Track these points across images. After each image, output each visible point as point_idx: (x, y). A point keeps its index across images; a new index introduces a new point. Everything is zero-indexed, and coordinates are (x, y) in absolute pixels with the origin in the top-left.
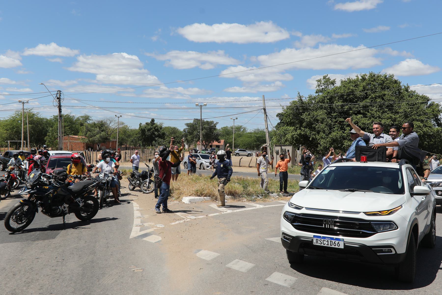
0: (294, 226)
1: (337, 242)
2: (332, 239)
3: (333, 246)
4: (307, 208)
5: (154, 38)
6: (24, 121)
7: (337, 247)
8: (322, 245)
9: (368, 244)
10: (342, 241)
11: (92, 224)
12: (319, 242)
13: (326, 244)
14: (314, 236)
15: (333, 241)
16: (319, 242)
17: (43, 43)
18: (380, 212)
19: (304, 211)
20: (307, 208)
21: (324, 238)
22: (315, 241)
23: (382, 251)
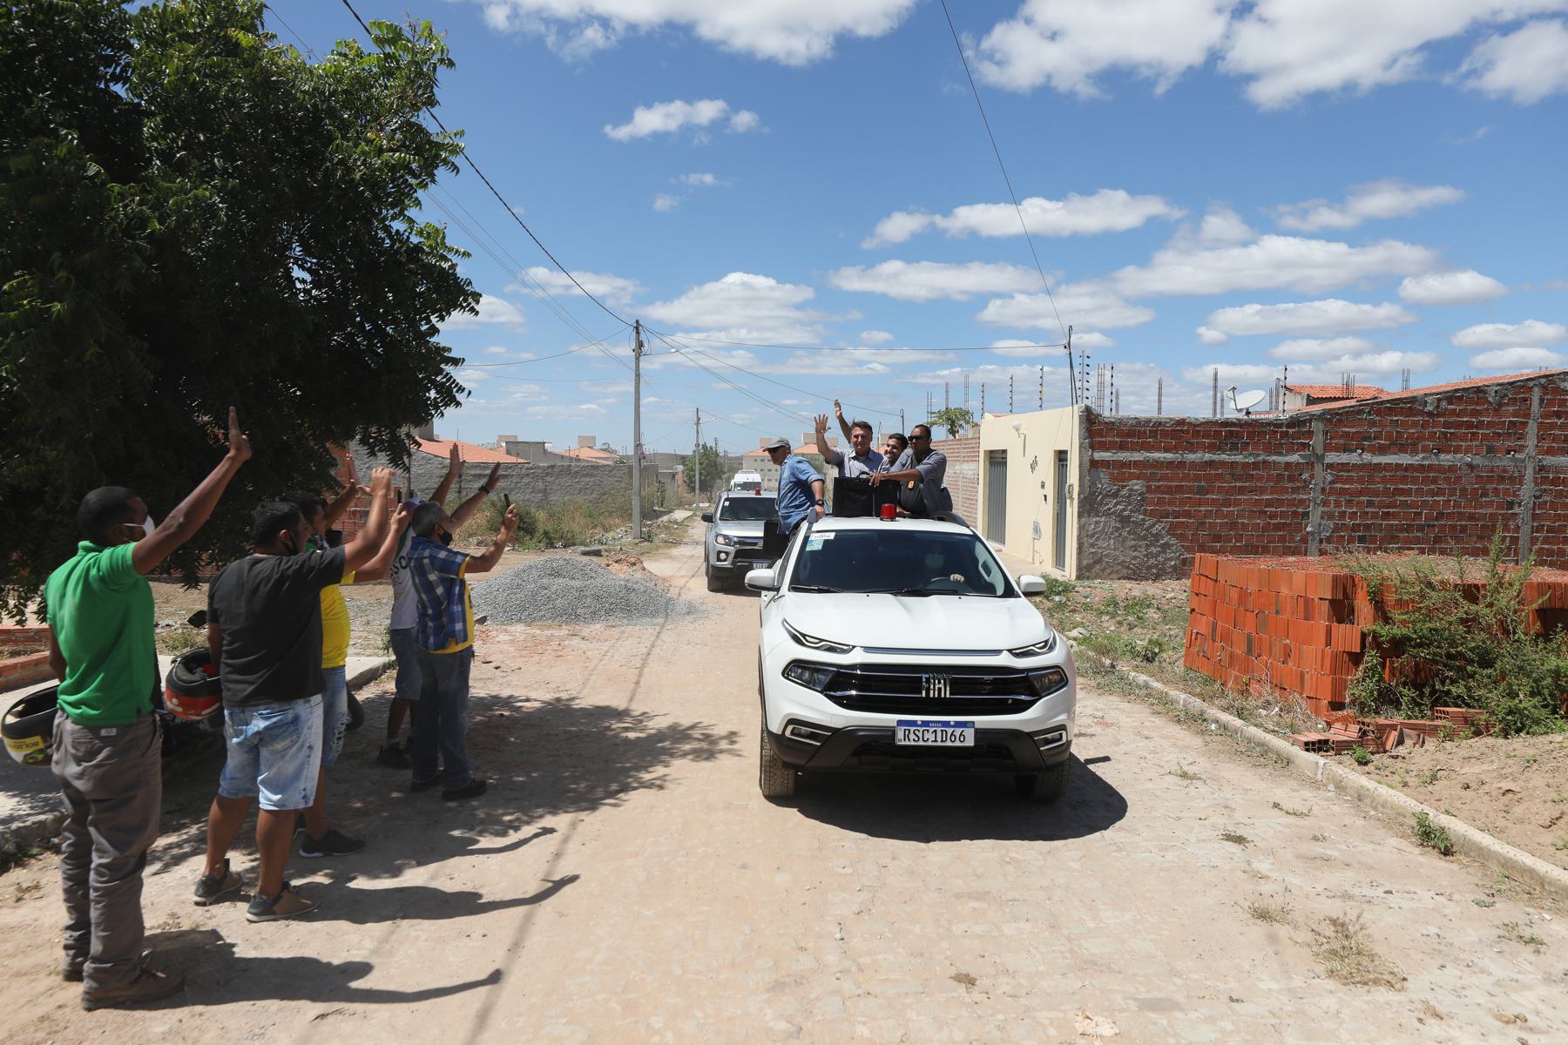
0: (838, 701)
1: (958, 731)
2: (946, 724)
3: (949, 743)
4: (868, 649)
5: (662, 203)
6: (1212, 448)
7: (958, 744)
8: (921, 743)
9: (1027, 729)
10: (961, 731)
11: (468, 858)
12: (912, 736)
13: (930, 739)
14: (900, 723)
15: (950, 730)
16: (912, 736)
17: (963, 204)
18: (804, 636)
19: (857, 657)
20: (868, 649)
21: (925, 724)
22: (900, 734)
23: (1048, 742)
